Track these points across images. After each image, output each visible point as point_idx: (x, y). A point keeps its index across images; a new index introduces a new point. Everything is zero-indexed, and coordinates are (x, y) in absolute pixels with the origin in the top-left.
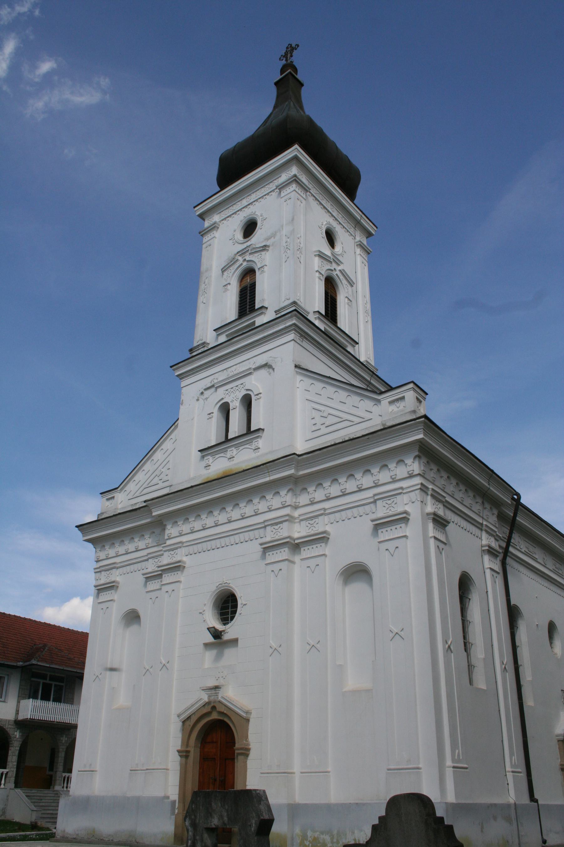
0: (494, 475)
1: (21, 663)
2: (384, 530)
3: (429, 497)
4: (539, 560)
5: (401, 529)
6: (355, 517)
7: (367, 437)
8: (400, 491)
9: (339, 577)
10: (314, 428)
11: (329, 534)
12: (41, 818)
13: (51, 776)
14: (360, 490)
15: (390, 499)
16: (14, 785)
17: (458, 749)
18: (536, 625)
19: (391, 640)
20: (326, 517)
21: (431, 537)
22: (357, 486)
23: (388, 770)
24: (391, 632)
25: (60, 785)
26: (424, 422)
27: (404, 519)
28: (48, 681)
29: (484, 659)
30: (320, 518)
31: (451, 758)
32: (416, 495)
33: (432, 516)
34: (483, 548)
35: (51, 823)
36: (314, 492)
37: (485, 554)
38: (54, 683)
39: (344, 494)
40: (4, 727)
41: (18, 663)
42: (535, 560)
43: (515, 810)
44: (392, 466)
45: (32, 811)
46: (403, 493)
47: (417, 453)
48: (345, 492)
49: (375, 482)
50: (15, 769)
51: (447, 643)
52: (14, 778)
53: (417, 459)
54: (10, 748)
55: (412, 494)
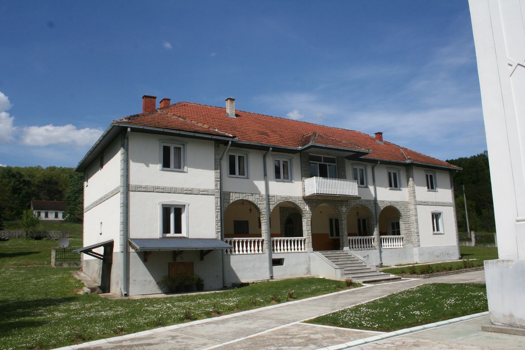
1: (300, 148)
12: (345, 274)
13: (338, 240)
16: (312, 249)
25: (347, 246)
27: (264, 204)
28: (323, 163)
35: (356, 278)
38: (328, 164)
40: (296, 203)
41: (297, 148)
45: (336, 269)
50: (311, 236)
52: (311, 244)
54: (303, 220)
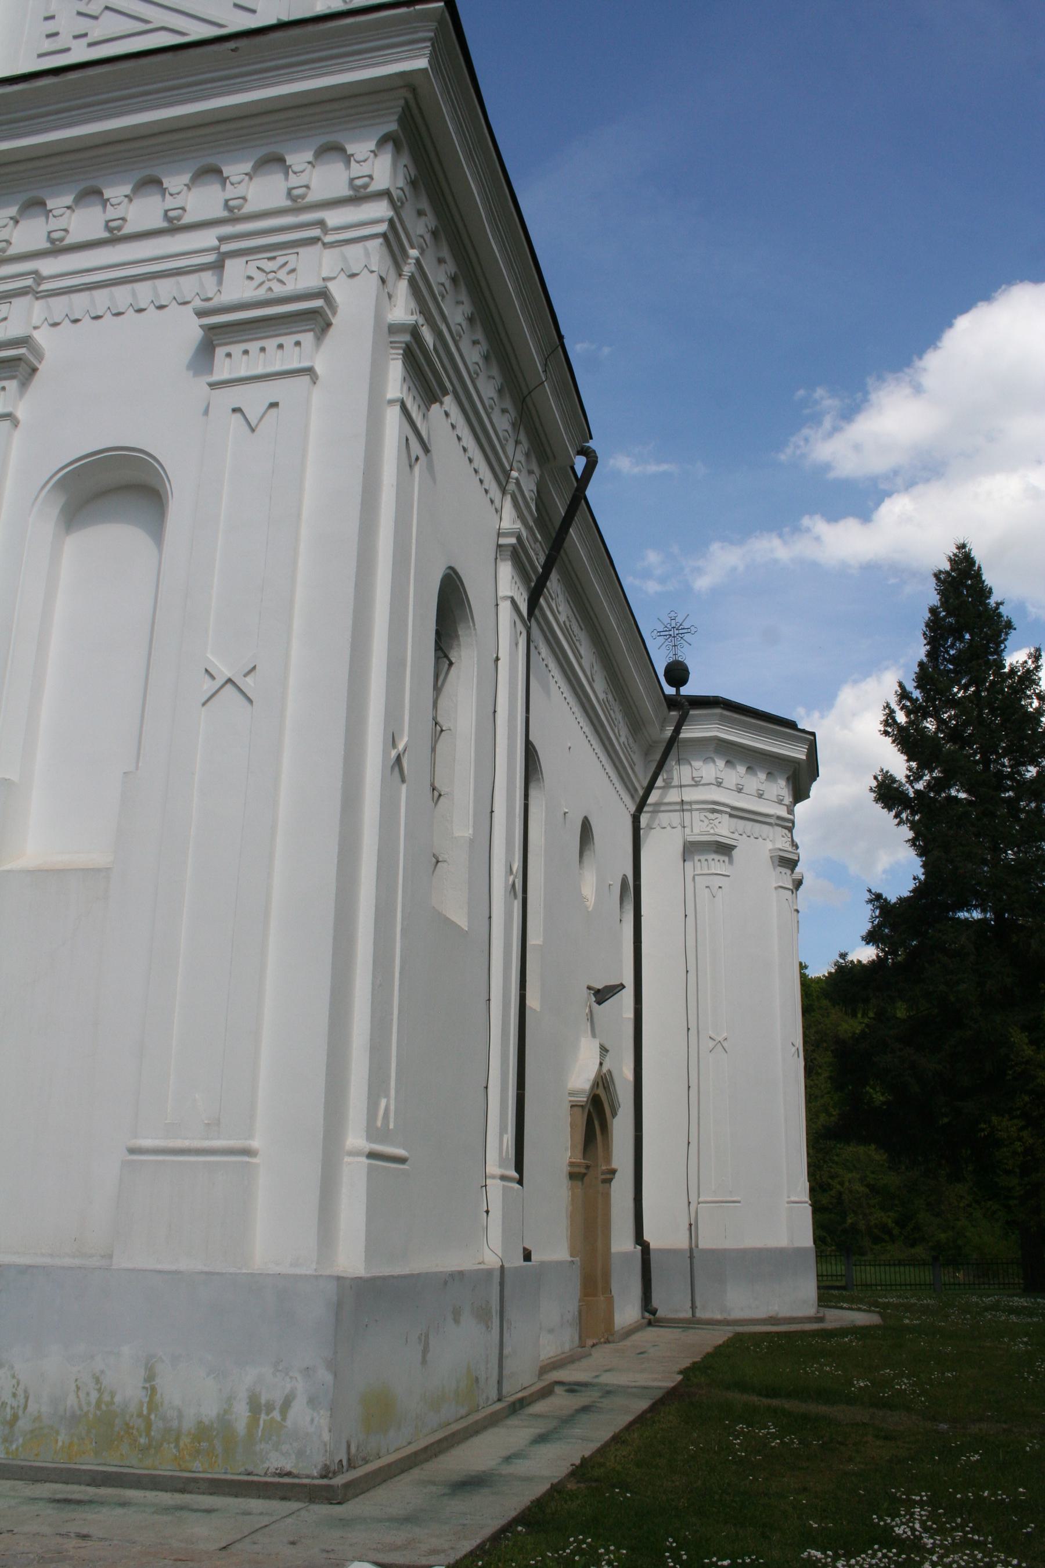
0: (560, 349)
2: (236, 349)
3: (403, 286)
4: (583, 662)
5: (297, 349)
6: (140, 311)
7: (232, 45)
8: (316, 232)
9: (49, 491)
10: (48, 45)
11: (40, 356)
14: (173, 227)
15: (274, 258)
17: (387, 1096)
18: (562, 813)
19: (204, 704)
20: (39, 305)
21: (391, 402)
22: (166, 211)
23: (132, 1151)
24: (207, 677)
26: (441, 22)
29: (472, 841)
30: (19, 303)
31: (364, 1124)
32: (367, 254)
33: (407, 338)
34: (503, 541)
36: (11, 223)
37: (502, 560)
39: (115, 237)
42: (578, 657)
43: (499, 1287)
44: (299, 159)
46: (324, 244)
47: (393, 126)
48: (119, 228)
49: (231, 203)
51: (394, 745)
53: (389, 147)
55: (356, 250)
